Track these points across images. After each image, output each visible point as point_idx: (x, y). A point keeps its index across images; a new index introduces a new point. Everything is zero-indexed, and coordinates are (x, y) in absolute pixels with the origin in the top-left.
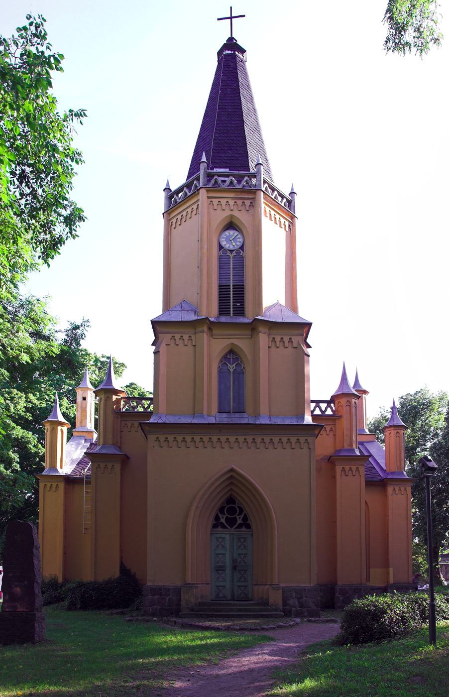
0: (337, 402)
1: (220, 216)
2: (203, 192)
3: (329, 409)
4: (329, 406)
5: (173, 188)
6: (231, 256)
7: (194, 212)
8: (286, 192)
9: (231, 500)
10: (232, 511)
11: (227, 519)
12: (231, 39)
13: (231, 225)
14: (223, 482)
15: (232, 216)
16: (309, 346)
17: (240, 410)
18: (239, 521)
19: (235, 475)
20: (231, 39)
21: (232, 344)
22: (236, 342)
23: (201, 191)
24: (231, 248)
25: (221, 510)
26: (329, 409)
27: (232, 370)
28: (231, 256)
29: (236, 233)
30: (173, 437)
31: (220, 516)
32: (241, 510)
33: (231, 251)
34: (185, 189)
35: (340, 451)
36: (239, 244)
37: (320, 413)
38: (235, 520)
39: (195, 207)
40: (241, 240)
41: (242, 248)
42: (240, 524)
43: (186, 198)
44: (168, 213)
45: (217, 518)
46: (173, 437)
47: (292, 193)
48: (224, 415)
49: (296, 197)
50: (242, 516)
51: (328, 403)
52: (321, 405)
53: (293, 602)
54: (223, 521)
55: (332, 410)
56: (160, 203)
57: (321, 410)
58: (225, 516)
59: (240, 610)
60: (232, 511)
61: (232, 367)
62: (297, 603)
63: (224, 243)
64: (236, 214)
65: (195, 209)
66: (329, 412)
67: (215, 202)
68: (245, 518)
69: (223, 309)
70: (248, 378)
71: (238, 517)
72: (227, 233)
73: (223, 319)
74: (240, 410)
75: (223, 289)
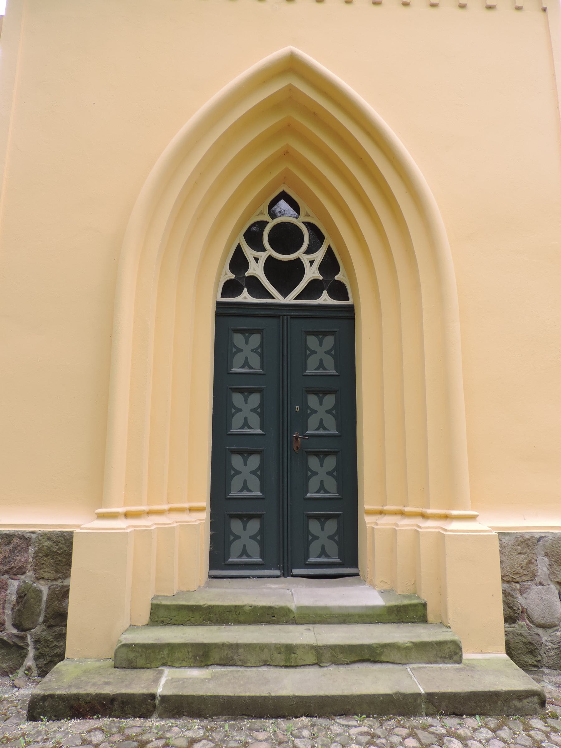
31: (249, 253)
50: (319, 256)
58: (263, 256)
71: (305, 259)
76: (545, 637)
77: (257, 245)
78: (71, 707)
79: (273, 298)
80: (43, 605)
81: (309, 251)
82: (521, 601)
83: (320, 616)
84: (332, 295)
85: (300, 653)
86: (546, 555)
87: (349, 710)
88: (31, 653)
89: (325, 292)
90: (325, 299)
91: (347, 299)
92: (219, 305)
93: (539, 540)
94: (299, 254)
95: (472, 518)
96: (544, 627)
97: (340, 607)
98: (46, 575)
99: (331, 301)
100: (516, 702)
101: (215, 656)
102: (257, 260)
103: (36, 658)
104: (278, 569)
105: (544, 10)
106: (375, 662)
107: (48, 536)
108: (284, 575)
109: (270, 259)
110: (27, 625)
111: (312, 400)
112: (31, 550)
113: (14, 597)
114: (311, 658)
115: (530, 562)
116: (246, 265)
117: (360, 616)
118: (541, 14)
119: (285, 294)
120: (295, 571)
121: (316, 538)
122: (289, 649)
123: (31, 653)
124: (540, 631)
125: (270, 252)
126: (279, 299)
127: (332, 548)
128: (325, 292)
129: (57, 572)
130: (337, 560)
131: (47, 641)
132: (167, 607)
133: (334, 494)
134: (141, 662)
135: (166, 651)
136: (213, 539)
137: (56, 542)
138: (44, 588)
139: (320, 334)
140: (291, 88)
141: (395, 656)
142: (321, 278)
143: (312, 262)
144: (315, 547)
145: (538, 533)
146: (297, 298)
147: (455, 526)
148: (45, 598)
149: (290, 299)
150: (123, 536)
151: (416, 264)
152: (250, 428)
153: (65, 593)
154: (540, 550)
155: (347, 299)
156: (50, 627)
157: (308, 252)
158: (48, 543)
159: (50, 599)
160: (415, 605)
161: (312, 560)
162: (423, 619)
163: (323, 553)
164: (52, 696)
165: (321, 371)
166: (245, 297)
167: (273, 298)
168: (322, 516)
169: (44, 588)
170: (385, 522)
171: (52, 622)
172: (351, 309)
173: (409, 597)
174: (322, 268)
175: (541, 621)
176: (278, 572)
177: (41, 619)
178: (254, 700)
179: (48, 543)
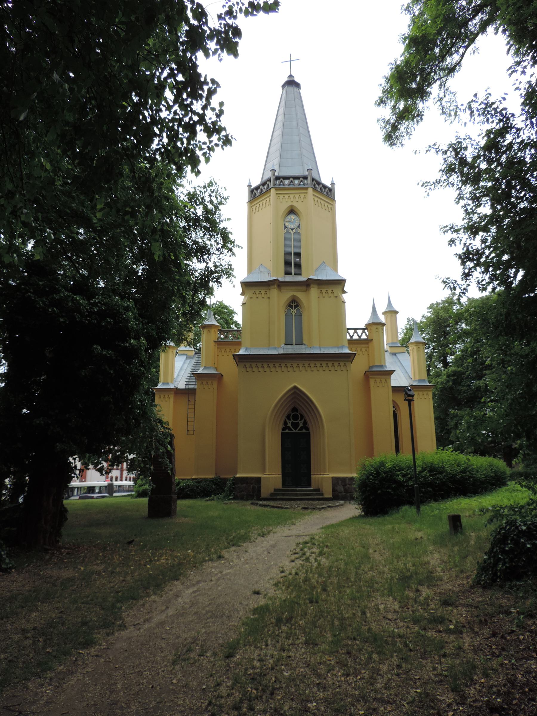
0: (369, 329)
1: (284, 206)
2: (273, 191)
3: (364, 334)
4: (364, 332)
5: (254, 185)
6: (292, 233)
7: (268, 204)
8: (328, 184)
9: (295, 409)
10: (295, 417)
11: (292, 424)
12: (291, 76)
13: (292, 211)
14: (290, 396)
15: (292, 206)
16: (344, 292)
17: (300, 343)
18: (301, 425)
19: (297, 391)
20: (291, 76)
21: (294, 296)
22: (296, 294)
23: (272, 190)
24: (292, 227)
25: (288, 417)
26: (364, 334)
27: (294, 314)
28: (292, 233)
29: (295, 216)
30: (331, 290)
31: (288, 421)
32: (302, 417)
33: (292, 229)
34: (261, 187)
35: (372, 367)
36: (298, 225)
37: (357, 338)
38: (298, 424)
39: (268, 199)
40: (298, 221)
41: (299, 227)
42: (302, 427)
43: (262, 194)
44: (250, 202)
45: (285, 423)
46: (331, 290)
47: (333, 184)
48: (289, 346)
49: (335, 186)
50: (302, 421)
51: (364, 329)
52: (358, 331)
53: (340, 488)
54: (289, 425)
55: (366, 335)
56: (245, 196)
57: (358, 335)
58: (291, 422)
59: (301, 495)
60: (295, 417)
61: (294, 311)
62: (343, 490)
63: (287, 224)
64: (295, 204)
65: (268, 201)
66: (364, 337)
67: (281, 196)
68: (305, 423)
69: (288, 272)
70: (305, 318)
71: (300, 422)
72: (289, 217)
73: (289, 278)
74: (300, 343)
75: (287, 256)
76: (340, 494)
77: (290, 420)
81: (300, 420)
84: (306, 430)
87: (185, 206)
90: (304, 431)
92: (282, 433)
116: (287, 424)
119: (295, 430)
126: (294, 431)
136: (282, 481)
138: (257, 487)
147: (325, 476)
149: (297, 431)
150: (269, 478)
157: (300, 420)
166: (287, 431)
169: (257, 487)
172: (309, 433)
174: (303, 424)
178: (285, 262)
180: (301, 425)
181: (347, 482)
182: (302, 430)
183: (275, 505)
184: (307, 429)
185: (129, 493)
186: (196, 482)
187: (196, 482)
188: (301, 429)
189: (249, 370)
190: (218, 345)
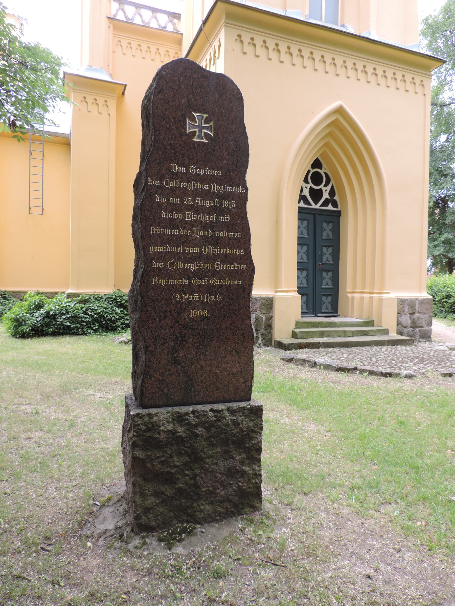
9: (317, 164)
18: (326, 195)
30: (287, 44)
50: (329, 188)
58: (309, 186)
71: (324, 189)
78: (299, 346)
79: (311, 205)
80: (264, 322)
81: (326, 185)
82: (400, 319)
83: (345, 324)
85: (348, 333)
86: (408, 305)
88: (260, 339)
89: (330, 204)
90: (330, 207)
91: (337, 207)
93: (406, 300)
94: (321, 187)
95: (389, 293)
96: (405, 327)
97: (351, 322)
98: (264, 312)
99: (332, 209)
100: (407, 342)
101: (325, 334)
102: (306, 188)
103: (262, 340)
104: (313, 314)
105: (425, 95)
106: (367, 335)
107: (264, 299)
108: (315, 316)
109: (311, 188)
110: (259, 329)
111: (325, 249)
112: (258, 303)
113: (254, 320)
114: (351, 335)
115: (403, 307)
117: (356, 324)
118: (423, 96)
119: (316, 203)
120: (319, 315)
121: (325, 303)
122: (345, 332)
123: (260, 339)
124: (404, 328)
125: (311, 185)
126: (314, 206)
127: (330, 306)
128: (330, 204)
129: (267, 311)
130: (331, 311)
131: (265, 334)
132: (301, 322)
133: (331, 287)
134: (305, 337)
135: (312, 333)
137: (267, 301)
138: (264, 317)
139: (328, 222)
140: (337, 119)
141: (373, 334)
142: (329, 198)
143: (326, 190)
144: (324, 306)
145: (406, 298)
146: (321, 206)
147: (384, 295)
148: (264, 320)
149: (318, 206)
151: (365, 196)
152: (303, 260)
153: (271, 318)
154: (406, 304)
155: (337, 207)
156: (266, 329)
157: (326, 185)
158: (264, 301)
159: (266, 320)
160: (371, 321)
161: (323, 311)
162: (373, 325)
163: (327, 308)
164: (294, 343)
165: (328, 238)
167: (311, 205)
168: (327, 295)
169: (264, 317)
170: (357, 296)
171: (267, 328)
172: (340, 212)
173: (368, 319)
175: (404, 325)
176: (313, 315)
177: (263, 327)
179: (264, 301)
180: (326, 195)
181: (417, 307)
182: (327, 206)
183: (334, 363)
184: (335, 204)
185: (176, 232)
186: (80, 302)
187: (80, 302)
188: (326, 203)
189: (248, 49)
190: (116, 28)
